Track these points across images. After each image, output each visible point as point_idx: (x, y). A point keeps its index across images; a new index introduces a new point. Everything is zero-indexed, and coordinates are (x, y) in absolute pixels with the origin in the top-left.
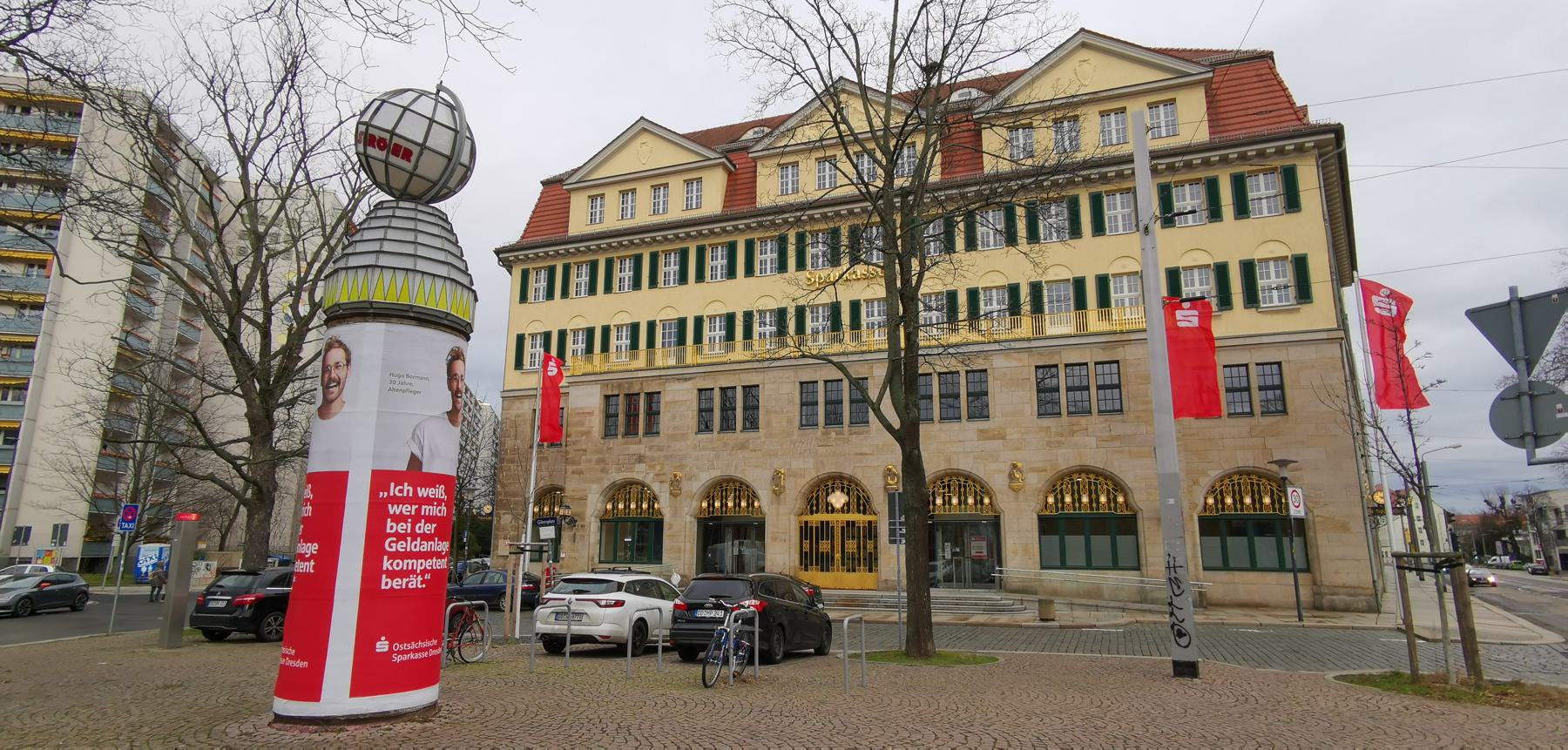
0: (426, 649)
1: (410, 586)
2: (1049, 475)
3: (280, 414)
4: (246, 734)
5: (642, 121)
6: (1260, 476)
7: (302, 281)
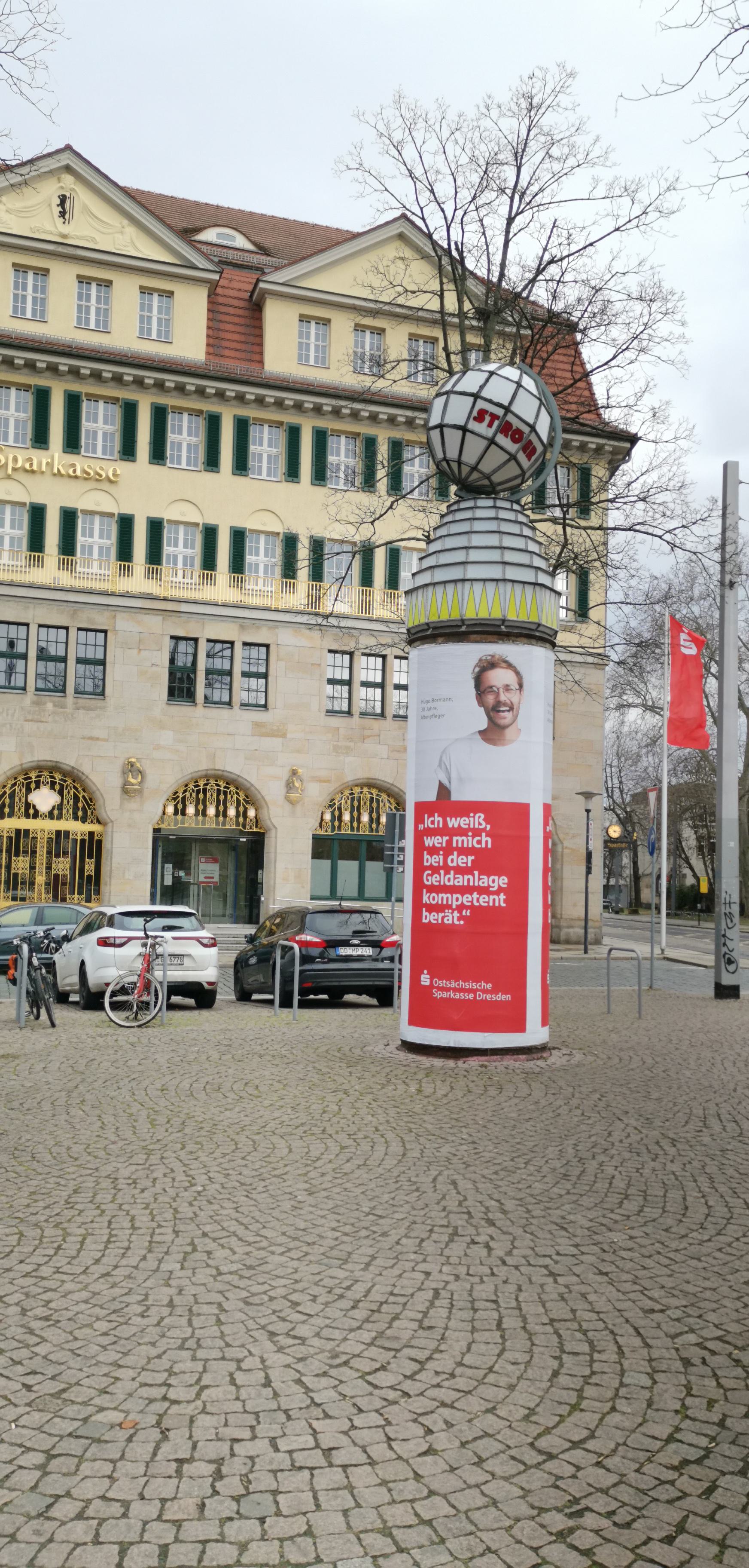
1: (446, 921)
2: (333, 787)
6: (381, 789)
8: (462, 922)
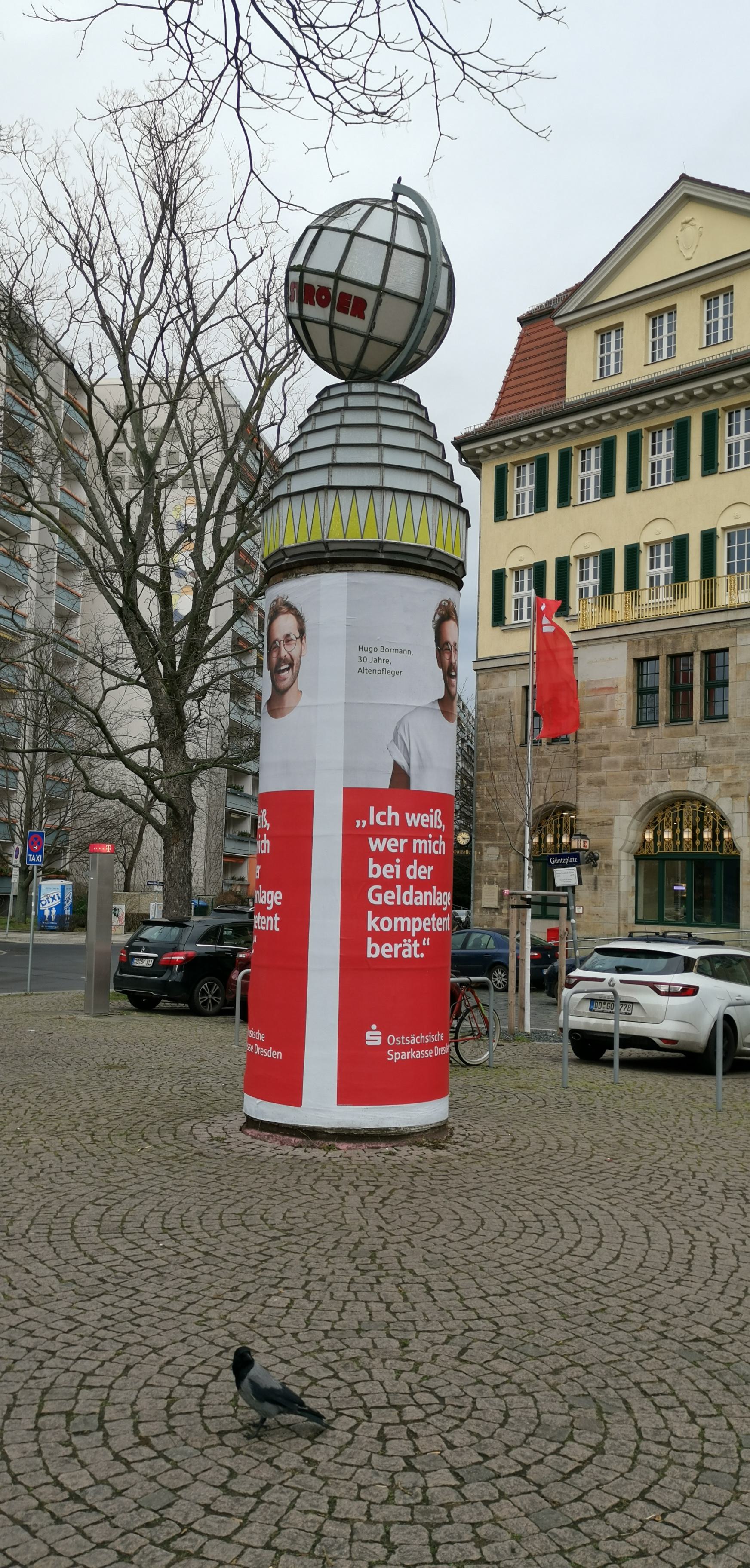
0: (430, 1046)
1: (404, 956)
3: (190, 707)
4: (218, 1139)
5: (684, 184)
7: (203, 518)
8: (422, 955)
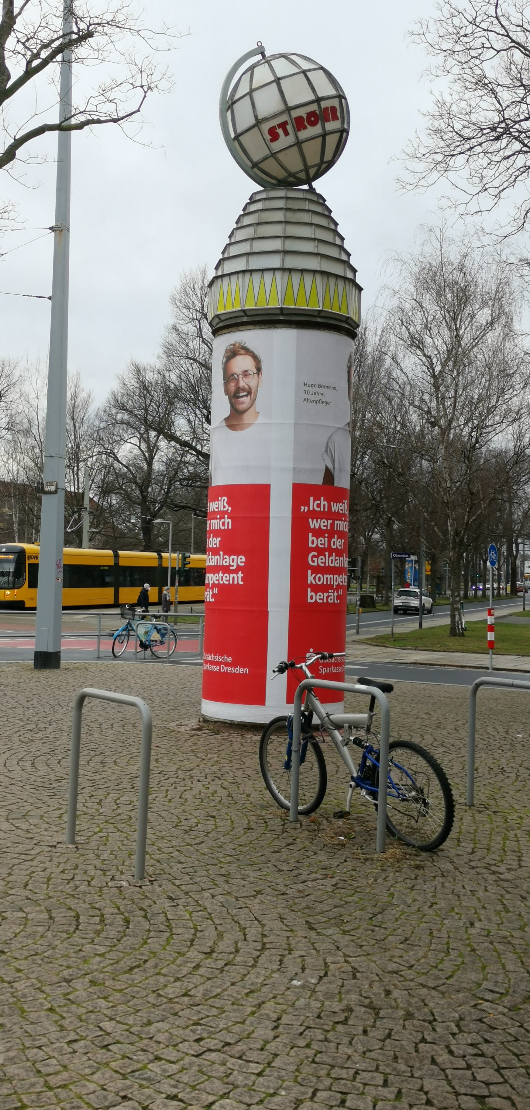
0: (218, 664)
1: (330, 601)
